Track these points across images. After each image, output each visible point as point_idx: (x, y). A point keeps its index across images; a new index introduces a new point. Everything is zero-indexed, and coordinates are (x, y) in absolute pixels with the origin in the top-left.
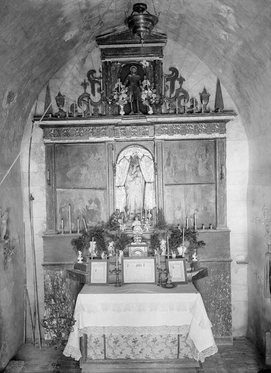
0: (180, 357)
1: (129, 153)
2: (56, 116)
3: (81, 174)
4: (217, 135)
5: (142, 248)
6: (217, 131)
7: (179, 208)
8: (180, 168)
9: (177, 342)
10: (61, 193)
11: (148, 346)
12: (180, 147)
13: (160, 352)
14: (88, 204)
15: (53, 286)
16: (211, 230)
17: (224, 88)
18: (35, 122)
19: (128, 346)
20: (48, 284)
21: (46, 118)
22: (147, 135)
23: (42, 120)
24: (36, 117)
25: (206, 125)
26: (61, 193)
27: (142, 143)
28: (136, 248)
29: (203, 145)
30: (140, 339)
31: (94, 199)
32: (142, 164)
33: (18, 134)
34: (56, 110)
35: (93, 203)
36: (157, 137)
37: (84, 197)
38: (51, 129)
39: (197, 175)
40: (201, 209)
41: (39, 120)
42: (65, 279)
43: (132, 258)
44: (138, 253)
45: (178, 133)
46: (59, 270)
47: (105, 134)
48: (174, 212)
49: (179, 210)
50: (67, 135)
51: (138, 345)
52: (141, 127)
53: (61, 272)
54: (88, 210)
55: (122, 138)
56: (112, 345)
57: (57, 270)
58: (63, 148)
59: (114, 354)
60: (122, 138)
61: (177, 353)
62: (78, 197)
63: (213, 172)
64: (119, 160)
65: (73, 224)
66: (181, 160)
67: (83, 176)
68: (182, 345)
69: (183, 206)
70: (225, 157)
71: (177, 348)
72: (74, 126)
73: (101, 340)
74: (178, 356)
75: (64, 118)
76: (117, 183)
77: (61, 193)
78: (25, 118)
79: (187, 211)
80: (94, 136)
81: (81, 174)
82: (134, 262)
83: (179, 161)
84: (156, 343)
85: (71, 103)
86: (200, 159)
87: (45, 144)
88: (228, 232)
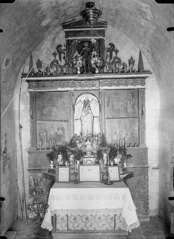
1: (83, 98)
3: (53, 112)
4: (139, 87)
5: (92, 159)
6: (140, 84)
8: (116, 108)
9: (114, 219)
11: (95, 222)
12: (116, 94)
13: (103, 225)
21: (30, 76)
22: (95, 86)
23: (28, 77)
24: (24, 75)
25: (133, 80)
27: (92, 92)
28: (88, 159)
31: (61, 127)
32: (92, 105)
33: (12, 86)
34: (36, 70)
35: (60, 130)
37: (54, 126)
39: (127, 112)
40: (129, 134)
41: (25, 77)
44: (89, 162)
45: (115, 85)
47: (68, 86)
55: (79, 88)
60: (79, 88)
62: (51, 126)
64: (77, 102)
67: (54, 112)
68: (117, 221)
69: (118, 132)
71: (114, 223)
73: (66, 218)
74: (115, 228)
75: (41, 75)
76: (75, 118)
78: (17, 75)
79: (120, 135)
82: (86, 168)
83: (115, 103)
84: (101, 219)
85: (46, 66)
86: (129, 102)
87: (30, 92)
88: (147, 149)
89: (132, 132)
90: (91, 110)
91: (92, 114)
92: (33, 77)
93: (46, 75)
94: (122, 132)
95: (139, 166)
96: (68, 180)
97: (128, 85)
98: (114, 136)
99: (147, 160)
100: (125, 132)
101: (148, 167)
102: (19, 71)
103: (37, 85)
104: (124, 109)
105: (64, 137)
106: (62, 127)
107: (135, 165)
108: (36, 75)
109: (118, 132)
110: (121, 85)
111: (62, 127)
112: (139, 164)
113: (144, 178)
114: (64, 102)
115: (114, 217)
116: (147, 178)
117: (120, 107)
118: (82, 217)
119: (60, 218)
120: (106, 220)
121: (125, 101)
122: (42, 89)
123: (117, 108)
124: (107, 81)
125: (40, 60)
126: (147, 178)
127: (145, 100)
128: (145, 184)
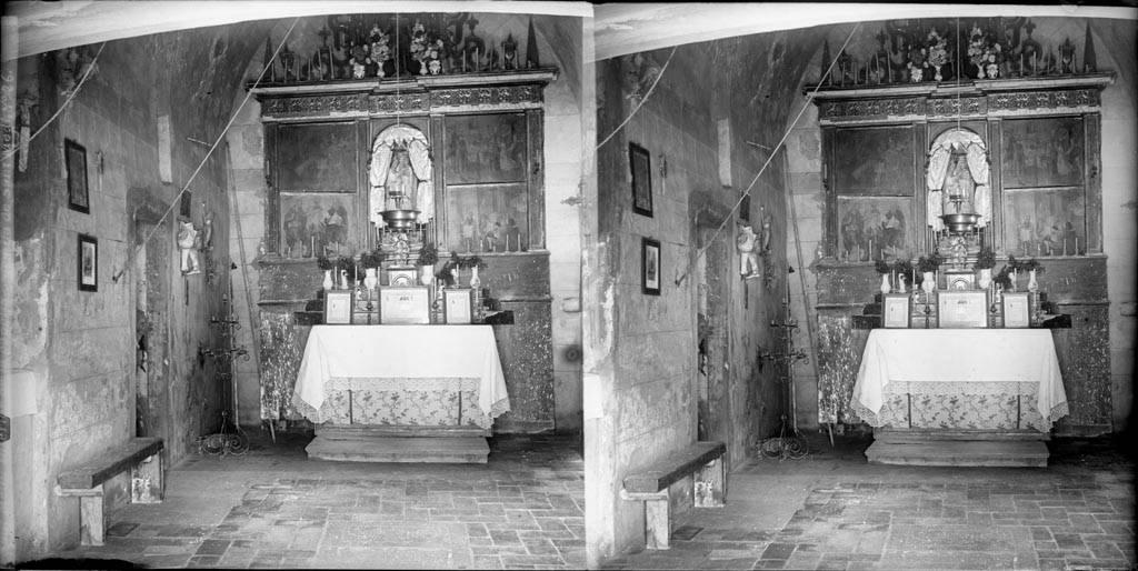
0: (1021, 427)
1: (953, 139)
2: (839, 84)
3: (318, 171)
4: (1085, 109)
5: (967, 277)
6: (528, 99)
7: (1027, 225)
8: (1029, 162)
9: (458, 399)
10: (845, 202)
11: (415, 405)
12: (471, 126)
13: (991, 418)
14: (327, 215)
15: (274, 336)
16: (519, 253)
17: (540, 34)
18: (809, 94)
19: (944, 409)
20: (824, 338)
21: (265, 82)
22: (420, 108)
23: (819, 90)
24: (810, 87)
25: (1068, 93)
26: (844, 203)
27: (969, 125)
28: (959, 276)
29: (1064, 126)
30: (402, 396)
31: (894, 211)
32: (413, 151)
33: (226, 110)
34: (838, 76)
35: (335, 216)
36: (990, 113)
37: (323, 205)
38: (272, 101)
39: (498, 168)
40: (1062, 226)
41: (813, 90)
42: (849, 330)
43: (951, 291)
44: (960, 284)
45: (1025, 106)
46: (841, 317)
47: (353, 107)
48: (1018, 230)
49: (470, 224)
50: (298, 109)
51: (958, 407)
52: (410, 96)
53: (287, 316)
54: (328, 226)
55: (938, 117)
56: (921, 407)
57: (281, 313)
58: (849, 134)
59: (923, 420)
60: (938, 117)
61: (457, 416)
62: (313, 205)
63: (1081, 167)
64: (375, 147)
65: (863, 251)
66: (1030, 150)
67: (878, 176)
68: (1024, 408)
69: (1033, 221)
70: (540, 140)
71: (1016, 413)
72: (307, 95)
73: (346, 396)
74: (459, 420)
75: (850, 86)
76: (931, 185)
77: (844, 203)
78: (793, 88)
79: (1039, 230)
80: (895, 113)
81: (318, 171)
82: (956, 298)
83: (1027, 151)
84: (371, 400)
85: (303, 63)
86: (503, 145)
87: (264, 123)
88: (547, 255)
89: (512, 217)
90: (411, 165)
91: (414, 174)
92: (830, 89)
93: (304, 82)
94: (486, 217)
95: (526, 297)
96: (469, 321)
97: (1057, 105)
98: (1023, 230)
99: (1106, 287)
100: (1051, 221)
101: (1108, 304)
102: (798, 80)
103: (838, 110)
104: (491, 161)
105: (345, 232)
106: (897, 211)
107: (1074, 298)
108: (839, 84)
109: (1033, 221)
110: (482, 102)
111: (897, 211)
112: (526, 293)
113: (541, 329)
114: (345, 146)
115: (1016, 398)
116: (1104, 330)
117: (1038, 159)
118: (942, 398)
119: (362, 395)
120: (440, 400)
121: (492, 141)
122: (294, 116)
123: (1031, 165)
124: (448, 93)
125: (847, 53)
126: (1104, 330)
127: (1100, 141)
128: (543, 343)
